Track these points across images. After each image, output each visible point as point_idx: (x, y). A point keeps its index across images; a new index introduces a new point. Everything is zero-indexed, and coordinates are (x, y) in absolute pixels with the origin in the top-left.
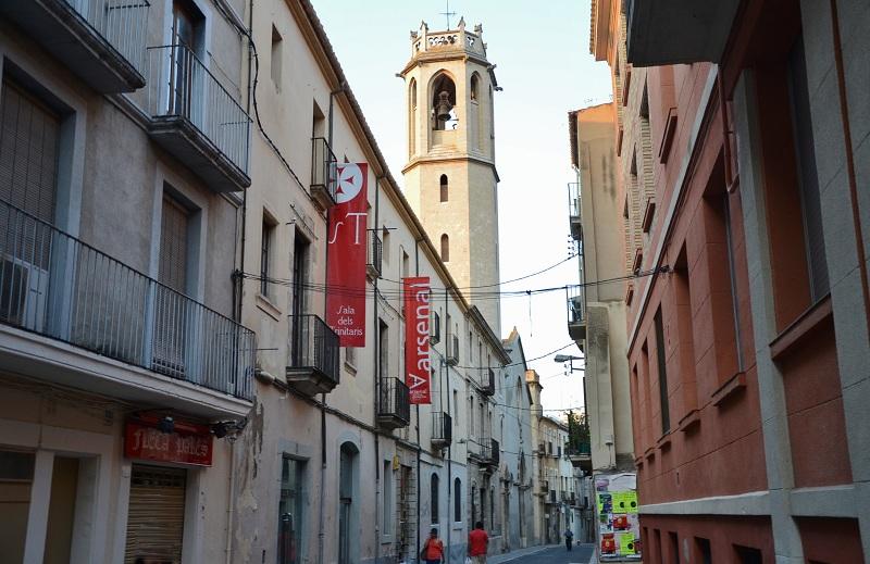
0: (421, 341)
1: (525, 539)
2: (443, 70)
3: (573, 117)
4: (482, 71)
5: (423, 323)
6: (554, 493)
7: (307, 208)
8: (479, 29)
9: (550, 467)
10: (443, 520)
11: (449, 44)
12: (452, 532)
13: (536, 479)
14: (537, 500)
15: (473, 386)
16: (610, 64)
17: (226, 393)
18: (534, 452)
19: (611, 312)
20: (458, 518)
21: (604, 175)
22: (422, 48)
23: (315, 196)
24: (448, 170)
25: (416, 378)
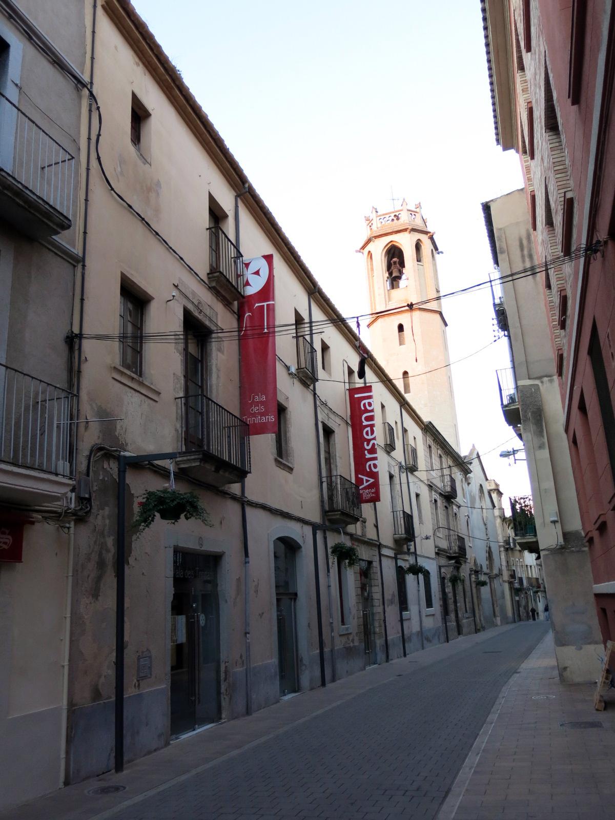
0: (368, 445)
1: (498, 619)
2: (391, 241)
3: (486, 208)
4: (425, 239)
5: (369, 429)
6: (521, 579)
7: (205, 297)
8: (419, 206)
9: (515, 557)
10: (413, 608)
11: (395, 221)
12: (424, 618)
13: (504, 568)
14: (506, 586)
15: (435, 491)
16: (517, 151)
17: (57, 474)
18: (500, 546)
19: (543, 389)
20: (429, 604)
21: (523, 256)
22: (374, 227)
23: (214, 284)
24: (404, 319)
25: (365, 478)
